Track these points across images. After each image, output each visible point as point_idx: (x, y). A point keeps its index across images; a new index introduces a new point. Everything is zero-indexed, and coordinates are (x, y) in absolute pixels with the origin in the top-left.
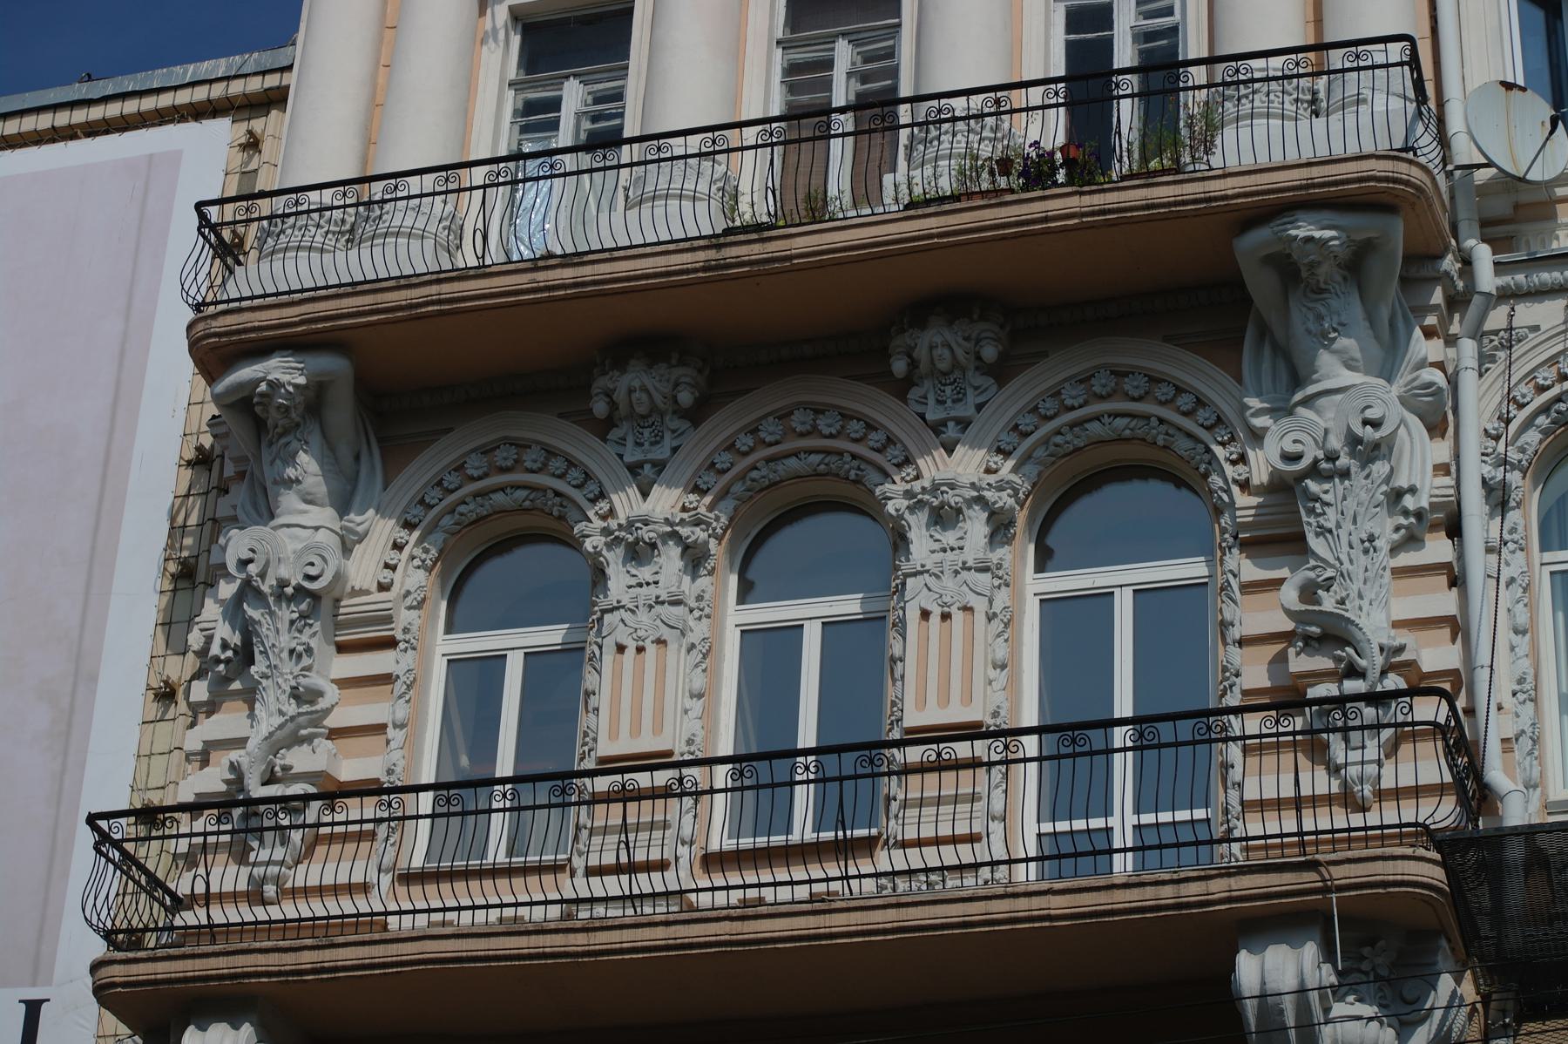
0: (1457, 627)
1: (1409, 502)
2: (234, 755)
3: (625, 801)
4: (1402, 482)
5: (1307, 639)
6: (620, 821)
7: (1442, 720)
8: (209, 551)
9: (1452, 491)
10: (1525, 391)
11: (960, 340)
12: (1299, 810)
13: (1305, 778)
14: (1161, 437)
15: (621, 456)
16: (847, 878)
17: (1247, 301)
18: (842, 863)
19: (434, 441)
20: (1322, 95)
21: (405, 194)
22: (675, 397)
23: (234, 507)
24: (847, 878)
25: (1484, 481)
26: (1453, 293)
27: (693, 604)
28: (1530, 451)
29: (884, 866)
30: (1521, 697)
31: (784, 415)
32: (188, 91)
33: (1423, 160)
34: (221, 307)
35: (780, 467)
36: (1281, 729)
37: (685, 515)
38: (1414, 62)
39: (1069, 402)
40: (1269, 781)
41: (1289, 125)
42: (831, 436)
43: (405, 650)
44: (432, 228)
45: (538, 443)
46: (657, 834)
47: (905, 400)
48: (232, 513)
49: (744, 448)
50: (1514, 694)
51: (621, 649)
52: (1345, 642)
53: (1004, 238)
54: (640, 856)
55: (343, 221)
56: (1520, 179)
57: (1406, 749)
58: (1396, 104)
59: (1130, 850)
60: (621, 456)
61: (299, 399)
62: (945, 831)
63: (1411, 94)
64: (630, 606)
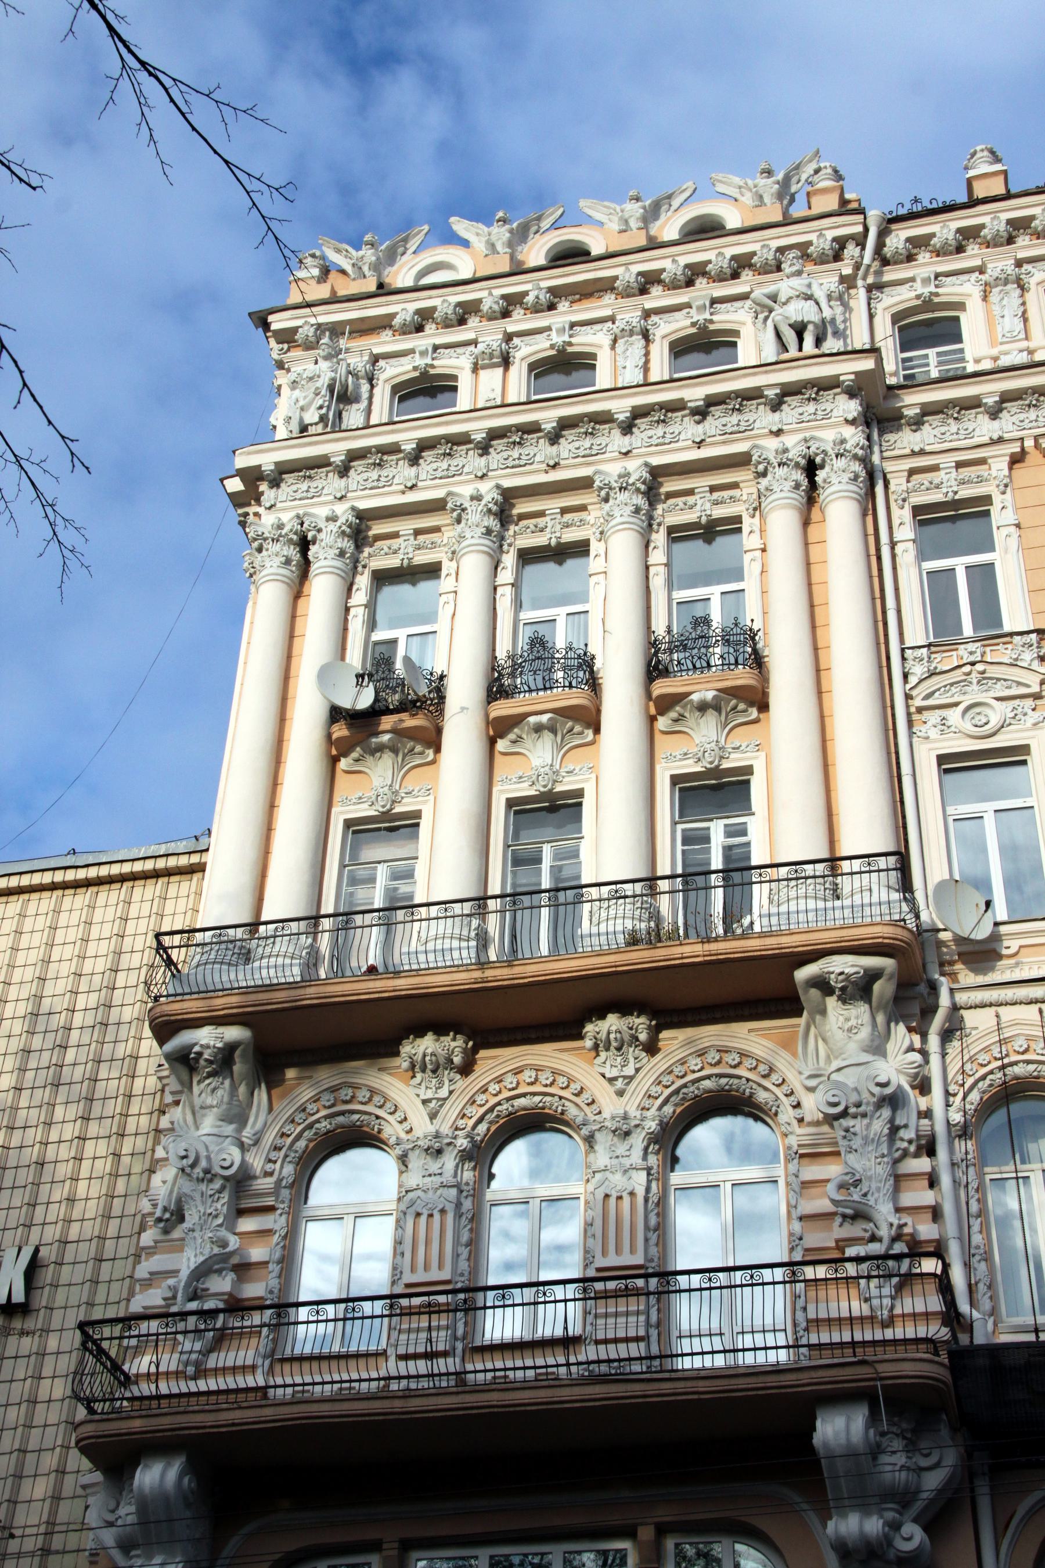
1: (903, 1134)
2: (171, 1282)
3: (430, 1313)
5: (844, 1216)
29: (582, 1358)
31: (518, 1071)
32: (152, 861)
42: (546, 1086)
46: (413, 1336)
51: (418, 1215)
52: (868, 1218)
57: (906, 1292)
59: (677, 1355)
62: (621, 1334)
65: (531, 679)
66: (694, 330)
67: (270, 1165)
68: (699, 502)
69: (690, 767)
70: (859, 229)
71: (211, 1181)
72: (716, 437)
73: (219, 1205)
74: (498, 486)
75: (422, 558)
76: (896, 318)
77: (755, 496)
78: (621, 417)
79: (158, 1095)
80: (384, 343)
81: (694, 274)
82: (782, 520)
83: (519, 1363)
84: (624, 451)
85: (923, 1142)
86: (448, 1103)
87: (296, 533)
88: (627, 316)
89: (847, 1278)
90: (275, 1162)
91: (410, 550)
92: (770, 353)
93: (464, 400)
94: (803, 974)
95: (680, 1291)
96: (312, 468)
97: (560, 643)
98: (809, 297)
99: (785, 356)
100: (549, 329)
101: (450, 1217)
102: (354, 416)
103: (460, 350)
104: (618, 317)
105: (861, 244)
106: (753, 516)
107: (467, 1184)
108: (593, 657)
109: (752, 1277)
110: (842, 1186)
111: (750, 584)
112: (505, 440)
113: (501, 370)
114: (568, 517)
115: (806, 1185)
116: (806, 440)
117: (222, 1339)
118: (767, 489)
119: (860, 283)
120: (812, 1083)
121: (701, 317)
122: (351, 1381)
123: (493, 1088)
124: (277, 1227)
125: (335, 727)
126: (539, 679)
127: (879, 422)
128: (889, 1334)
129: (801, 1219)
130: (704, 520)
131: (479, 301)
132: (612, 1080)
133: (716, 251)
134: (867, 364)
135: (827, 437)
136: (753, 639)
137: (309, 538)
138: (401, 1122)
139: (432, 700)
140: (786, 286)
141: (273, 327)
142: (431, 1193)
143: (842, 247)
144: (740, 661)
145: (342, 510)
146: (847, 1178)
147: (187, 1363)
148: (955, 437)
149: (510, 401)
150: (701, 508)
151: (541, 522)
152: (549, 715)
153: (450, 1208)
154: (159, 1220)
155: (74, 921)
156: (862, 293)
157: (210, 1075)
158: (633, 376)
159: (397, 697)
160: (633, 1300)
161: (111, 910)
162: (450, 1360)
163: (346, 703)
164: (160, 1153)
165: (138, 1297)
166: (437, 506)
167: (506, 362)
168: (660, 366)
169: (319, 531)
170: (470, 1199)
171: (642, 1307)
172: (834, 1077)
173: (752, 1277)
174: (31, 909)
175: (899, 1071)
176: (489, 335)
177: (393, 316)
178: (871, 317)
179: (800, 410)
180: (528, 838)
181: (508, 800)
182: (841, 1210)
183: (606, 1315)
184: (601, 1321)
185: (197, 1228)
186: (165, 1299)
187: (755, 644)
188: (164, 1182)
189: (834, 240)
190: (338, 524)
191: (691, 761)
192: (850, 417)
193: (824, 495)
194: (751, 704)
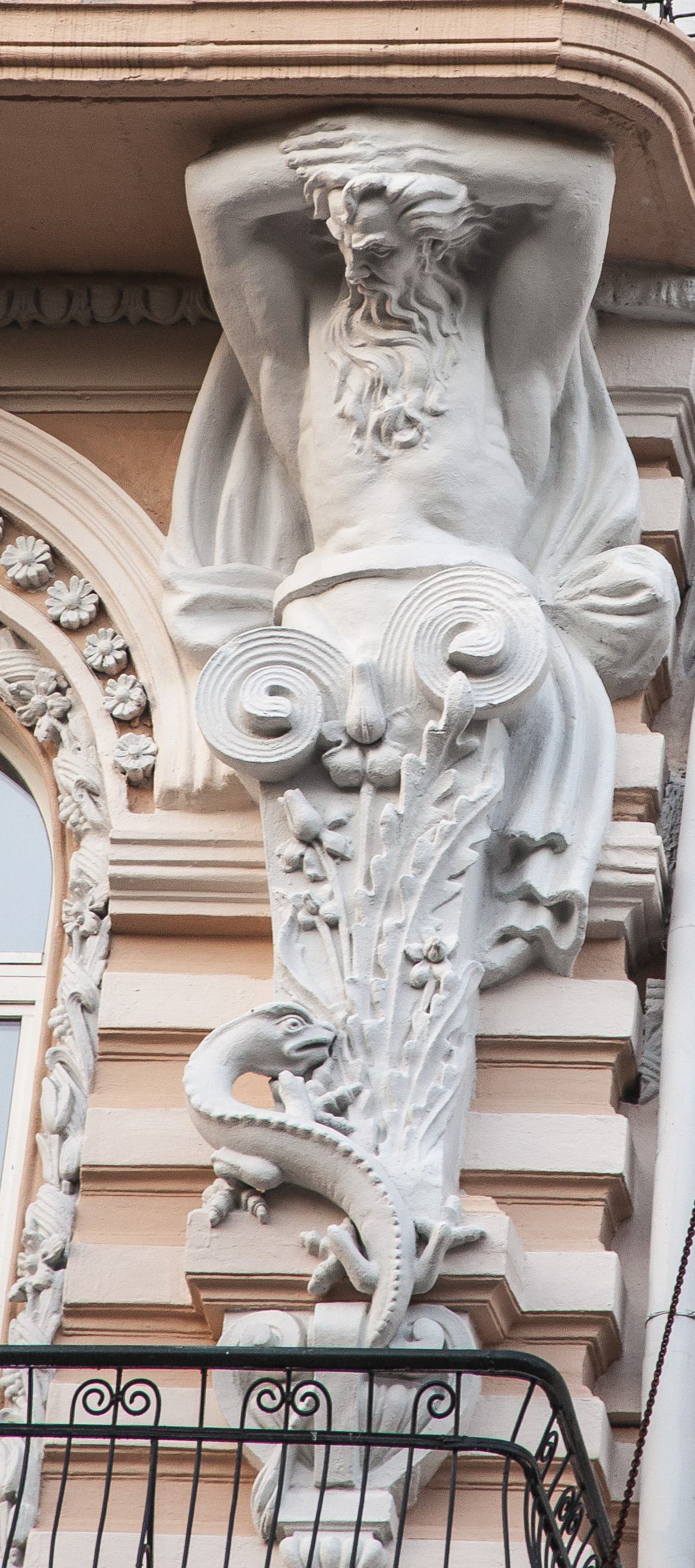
0: (623, 1212)
1: (541, 874)
4: (531, 824)
5: (239, 1186)
7: (530, 1440)
9: (651, 861)
17: (209, 330)
36: (124, 1419)
85: (621, 915)
94: (217, 182)
110: (259, 1062)
115: (122, 1045)
129: (75, 1182)
146: (276, 1030)
172: (297, 615)
175: (555, 614)
182: (225, 1159)
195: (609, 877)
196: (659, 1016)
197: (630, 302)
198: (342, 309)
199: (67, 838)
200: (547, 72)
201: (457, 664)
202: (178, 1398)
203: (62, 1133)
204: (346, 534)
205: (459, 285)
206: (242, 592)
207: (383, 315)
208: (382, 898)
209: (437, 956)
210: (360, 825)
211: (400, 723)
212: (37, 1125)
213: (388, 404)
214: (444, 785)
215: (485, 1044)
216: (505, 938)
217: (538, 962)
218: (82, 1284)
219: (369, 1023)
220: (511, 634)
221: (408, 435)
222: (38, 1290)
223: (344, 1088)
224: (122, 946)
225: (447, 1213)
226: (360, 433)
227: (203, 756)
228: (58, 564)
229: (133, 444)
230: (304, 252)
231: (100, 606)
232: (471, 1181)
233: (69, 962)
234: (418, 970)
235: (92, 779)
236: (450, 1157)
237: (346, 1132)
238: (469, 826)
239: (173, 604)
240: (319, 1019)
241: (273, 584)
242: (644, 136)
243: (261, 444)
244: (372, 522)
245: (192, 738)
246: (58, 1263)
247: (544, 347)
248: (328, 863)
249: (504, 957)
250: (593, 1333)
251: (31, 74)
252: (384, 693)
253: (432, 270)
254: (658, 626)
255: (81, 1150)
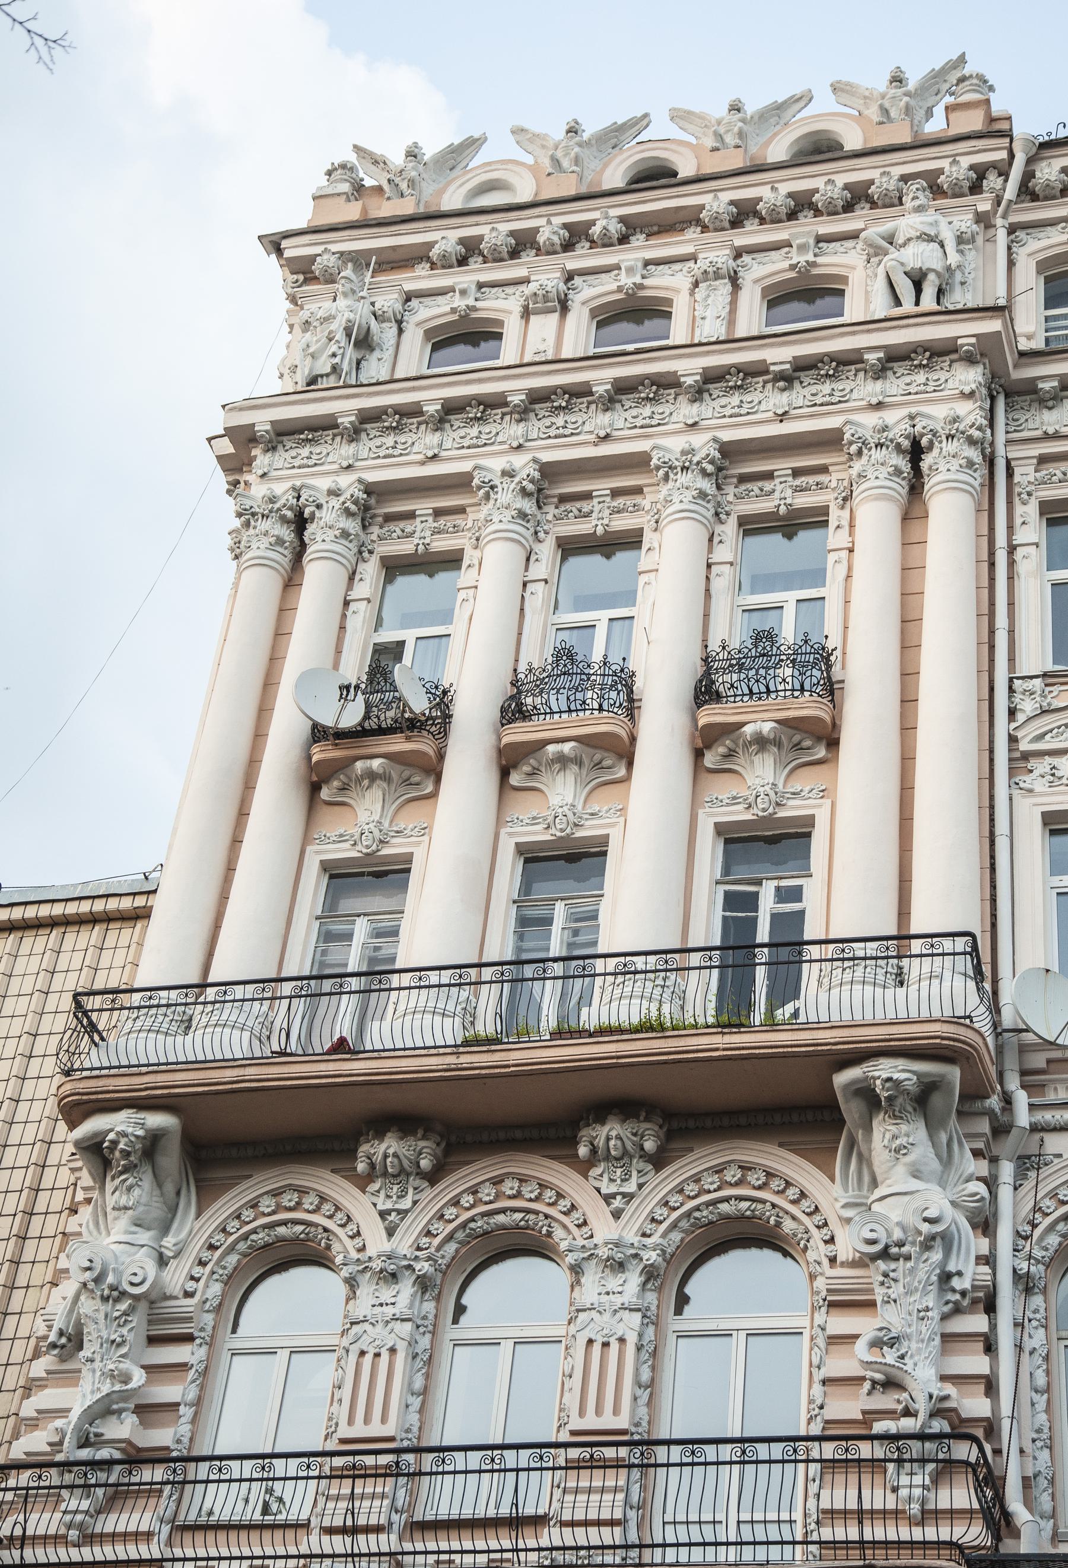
0: (990, 1386)
1: (956, 1283)
2: (59, 1423)
3: (354, 1477)
4: (952, 1267)
5: (874, 1382)
6: (349, 1491)
8: (57, 1258)
10: (1048, 1203)
11: (629, 1135)
12: (861, 1522)
13: (866, 1493)
14: (773, 1218)
15: (375, 1205)
16: (517, 1550)
17: (843, 1122)
18: (514, 1534)
19: (238, 1184)
20: (905, 970)
21: (231, 998)
22: (418, 1163)
23: (81, 1225)
24: (517, 1550)
25: (1014, 1270)
26: (996, 1125)
27: (419, 1322)
28: (1052, 1250)
29: (544, 1542)
30: (1039, 1444)
31: (497, 1181)
33: (976, 1025)
34: (85, 1074)
35: (492, 1221)
36: (850, 1457)
37: (418, 1253)
38: (974, 951)
39: (706, 1187)
40: (839, 1493)
41: (879, 991)
42: (531, 1200)
43: (201, 1345)
44: (250, 1023)
45: (315, 1190)
47: (586, 1177)
48: (78, 1229)
49: (467, 1205)
50: (1034, 1441)
51: (363, 1353)
53: (665, 1062)
54: (362, 1521)
55: (184, 1013)
56: (1051, 1043)
58: (959, 981)
60: (375, 1205)
61: (139, 1146)
63: (971, 973)
64: (373, 1321)
65: (553, 698)
66: (793, 274)
67: (192, 1283)
68: (779, 488)
69: (739, 814)
70: (1003, 155)
71: (117, 1300)
72: (802, 410)
73: (124, 1331)
74: (535, 460)
75: (442, 544)
76: (1042, 266)
77: (846, 483)
78: (689, 381)
79: (70, 1191)
80: (420, 278)
81: (802, 205)
82: (875, 518)
83: (468, 1545)
84: (690, 422)
85: (981, 1294)
86: (635, 1202)
87: (290, 509)
88: (712, 256)
89: (859, 1461)
90: (198, 1280)
91: (428, 533)
92: (881, 307)
93: (509, 352)
94: (843, 1078)
95: (656, 1465)
96: (316, 430)
97: (597, 656)
98: (931, 239)
99: (898, 311)
100: (618, 267)
101: (400, 1357)
102: (376, 368)
103: (509, 290)
104: (701, 256)
105: (1004, 174)
106: (843, 508)
107: (425, 1318)
108: (633, 674)
109: (744, 1452)
110: (877, 1344)
111: (832, 591)
112: (548, 404)
113: (556, 316)
114: (620, 501)
115: (836, 1340)
116: (912, 417)
117: (119, 1496)
118: (859, 476)
119: (999, 221)
120: (849, 1213)
121: (801, 259)
122: (450, 1552)
123: (467, 1200)
124: (193, 1360)
125: (315, 749)
126: (563, 698)
127: (1007, 396)
128: (917, 1534)
129: (824, 1382)
130: (783, 510)
131: (536, 230)
132: (608, 1198)
133: (826, 178)
134: (993, 325)
135: (937, 414)
136: (828, 659)
137: (306, 515)
138: (352, 1237)
139: (434, 719)
140: (908, 223)
141: (287, 254)
142: (380, 1326)
143: (981, 177)
144: (807, 686)
145: (346, 481)
146: (881, 1334)
147: (69, 1527)
148: (305, 461)
149: (564, 356)
150: (781, 495)
151: (585, 506)
152: (572, 744)
153: (401, 1347)
154: (54, 1346)
155: (33, 968)
156: (1002, 235)
157: (125, 1170)
158: (712, 329)
159: (391, 714)
160: (598, 1473)
161: (35, 960)
162: (383, 1537)
163: (328, 721)
164: (63, 1263)
165: (22, 1440)
166: (461, 483)
167: (564, 306)
168: (751, 316)
169: (319, 507)
170: (205, 1348)
171: (621, 1483)
172: (875, 1207)
173: (744, 1452)
174: (68, 944)
175: (953, 1203)
176: (545, 274)
177: (430, 245)
178: (1011, 264)
179: (908, 379)
180: (542, 890)
181: (717, 825)
182: (869, 1374)
183: (577, 1491)
184: (569, 1498)
185: (98, 1357)
186: (50, 1444)
187: (829, 667)
188: (64, 1298)
189: (972, 167)
190: (342, 499)
191: (740, 807)
192: (967, 390)
193: (931, 484)
194: (819, 739)
195: (976, 1283)
196: (996, 1325)
197: (966, 1108)
198: (882, 1114)
199: (812, 1277)
200: (938, 1041)
201: (926, 1220)
202: (865, 1450)
203: (819, 1367)
204: (888, 1182)
205: (916, 1105)
206: (858, 1201)
207: (894, 1115)
208: (909, 1292)
209: (927, 1309)
210: (901, 1269)
211: (910, 1239)
212: (811, 1365)
213: (898, 1142)
214: (925, 1257)
215: (943, 1335)
216: (947, 1303)
217: (958, 1310)
218: (829, 1414)
219: (908, 1331)
220: (942, 1212)
221: (905, 1151)
222: (816, 1416)
223: (903, 1351)
224: (831, 1310)
225: (938, 1389)
226: (890, 1151)
227: (851, 1251)
228: (803, 1195)
229: (822, 1158)
230: (868, 1096)
231: (816, 1207)
232: (944, 1378)
233: (816, 1315)
234: (922, 1314)
235: (818, 1259)
236: (937, 1371)
237: (905, 1364)
238: (934, 1269)
239: (838, 1205)
240: (893, 1330)
241: (868, 1198)
242: (968, 1058)
243: (860, 1156)
244: (896, 1178)
245: (847, 1245)
246: (821, 1407)
247: (943, 1123)
248: (892, 1282)
249: (946, 1309)
250: (985, 1424)
251: (785, 1050)
252: (904, 1229)
253: (908, 1101)
254: (984, 1205)
255: (824, 1373)
